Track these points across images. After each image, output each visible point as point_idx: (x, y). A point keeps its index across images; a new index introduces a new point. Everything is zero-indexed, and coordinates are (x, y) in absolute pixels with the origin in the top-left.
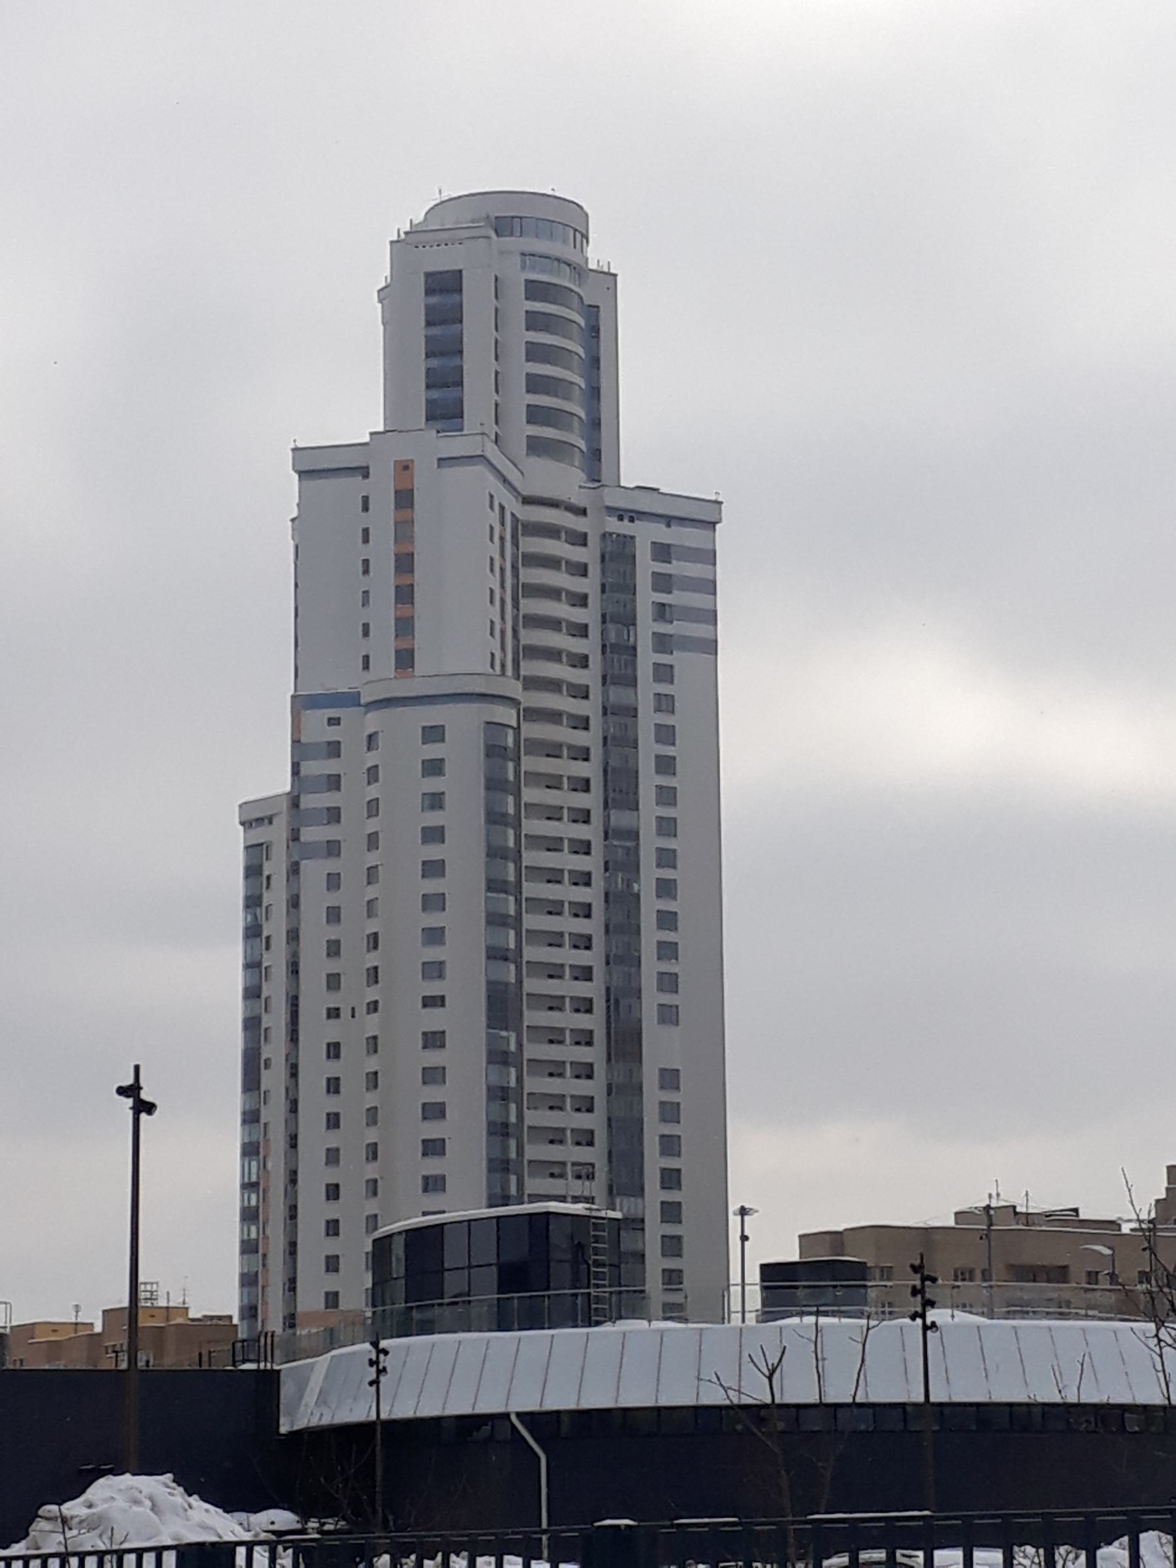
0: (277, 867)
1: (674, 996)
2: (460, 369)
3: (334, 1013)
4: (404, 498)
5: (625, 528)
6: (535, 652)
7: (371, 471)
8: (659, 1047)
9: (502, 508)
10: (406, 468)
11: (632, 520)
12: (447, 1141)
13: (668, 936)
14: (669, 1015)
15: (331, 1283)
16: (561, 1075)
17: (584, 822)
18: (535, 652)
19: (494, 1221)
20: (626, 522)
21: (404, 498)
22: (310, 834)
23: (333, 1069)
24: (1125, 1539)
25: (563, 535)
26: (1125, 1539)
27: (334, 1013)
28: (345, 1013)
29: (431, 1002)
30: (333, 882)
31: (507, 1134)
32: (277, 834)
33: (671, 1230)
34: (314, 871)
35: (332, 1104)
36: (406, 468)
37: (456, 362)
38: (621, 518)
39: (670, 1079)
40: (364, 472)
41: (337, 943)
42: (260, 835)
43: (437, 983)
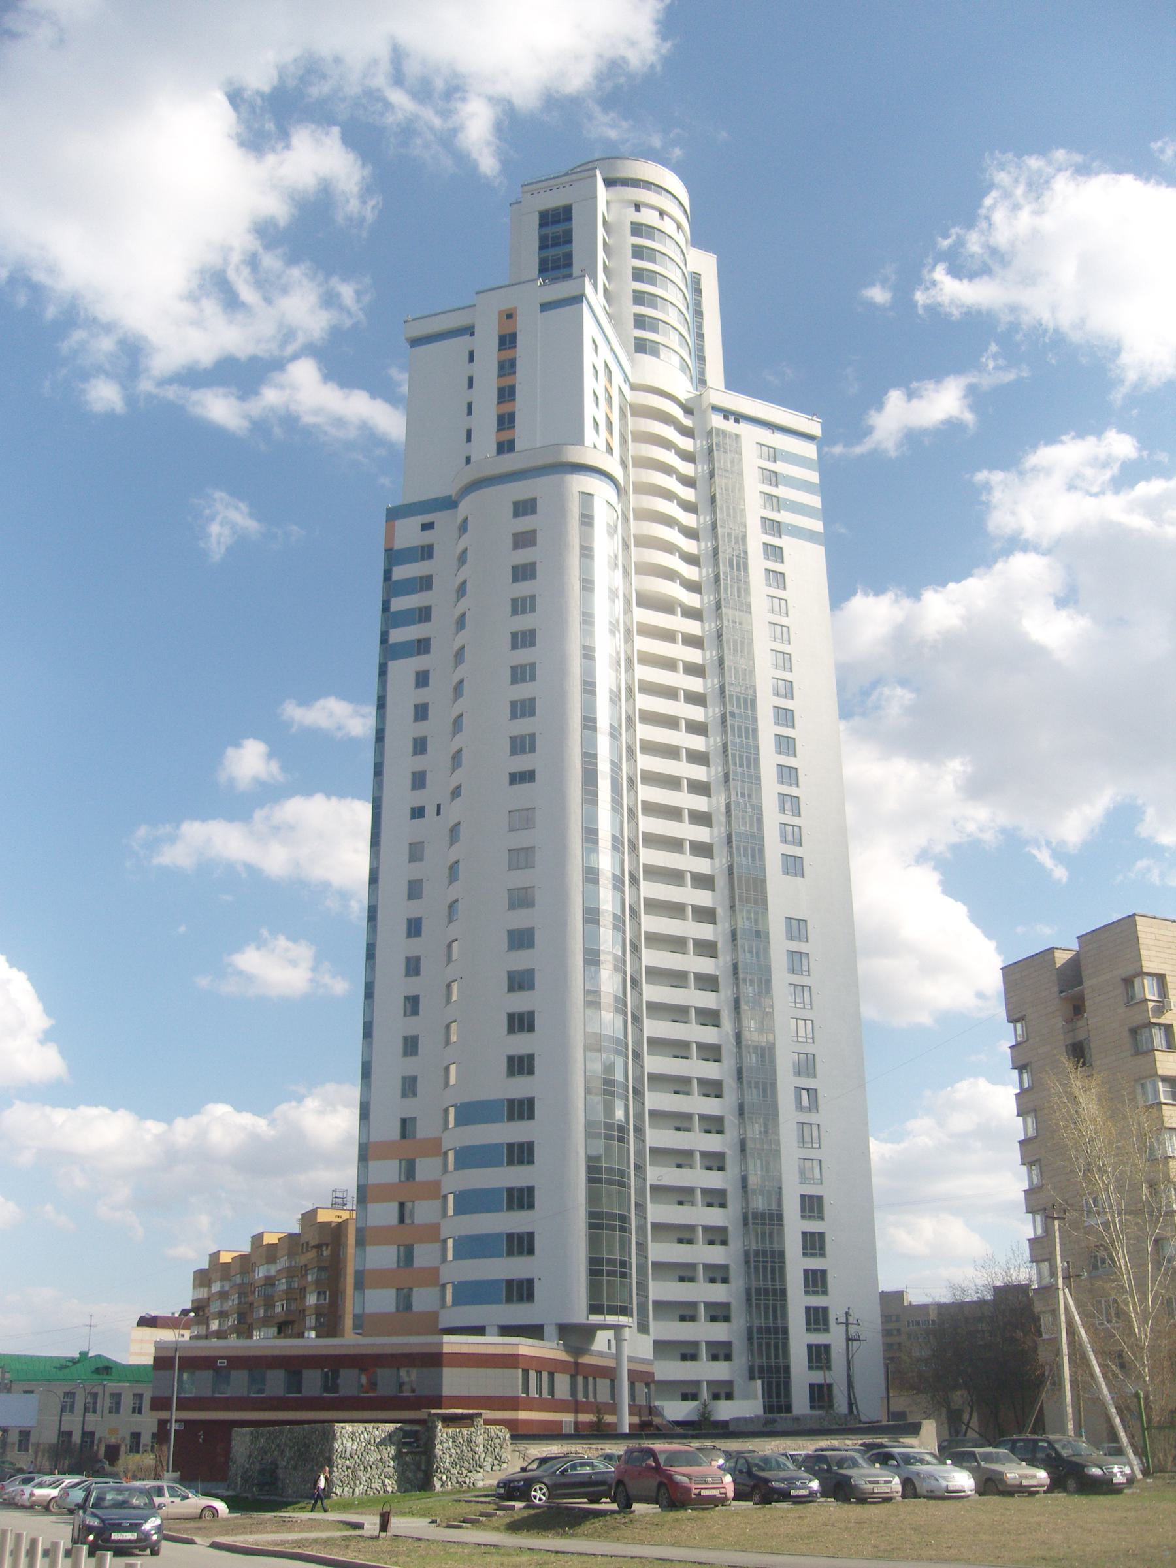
1: (823, 1298)
2: (571, 231)
4: (507, 341)
5: (730, 426)
6: (645, 542)
7: (476, 330)
8: (783, 897)
10: (510, 316)
11: (737, 421)
12: (536, 1281)
14: (794, 866)
16: (692, 1280)
17: (717, 1096)
18: (645, 542)
19: (588, 1054)
20: (732, 421)
21: (507, 341)
29: (517, 778)
30: (422, 679)
31: (612, 1094)
33: (814, 1264)
36: (510, 316)
37: (566, 248)
38: (726, 418)
39: (797, 928)
40: (470, 331)
43: (517, 697)
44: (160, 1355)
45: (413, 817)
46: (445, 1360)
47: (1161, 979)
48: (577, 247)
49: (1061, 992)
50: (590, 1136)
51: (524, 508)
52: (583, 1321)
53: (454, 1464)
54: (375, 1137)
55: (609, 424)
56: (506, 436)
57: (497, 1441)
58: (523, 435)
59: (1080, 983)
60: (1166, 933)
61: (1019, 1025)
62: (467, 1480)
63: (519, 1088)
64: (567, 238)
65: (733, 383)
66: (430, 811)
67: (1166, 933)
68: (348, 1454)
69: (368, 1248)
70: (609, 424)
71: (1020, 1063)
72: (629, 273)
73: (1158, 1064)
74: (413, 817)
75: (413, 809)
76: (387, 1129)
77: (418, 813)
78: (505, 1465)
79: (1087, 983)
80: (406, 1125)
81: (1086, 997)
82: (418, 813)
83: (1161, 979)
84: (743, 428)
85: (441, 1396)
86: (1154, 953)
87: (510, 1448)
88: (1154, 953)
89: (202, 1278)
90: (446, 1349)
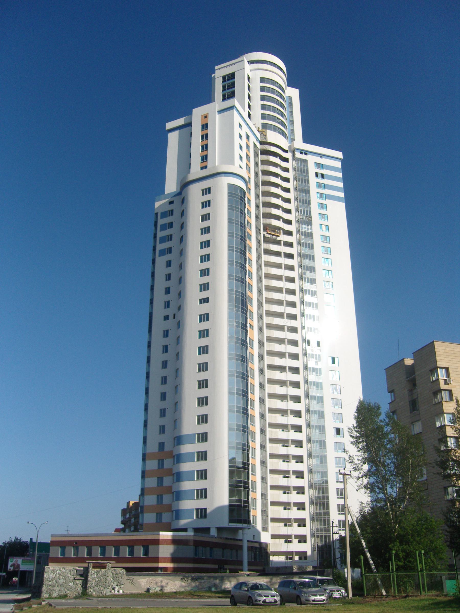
5: (303, 157)
10: (206, 117)
15: (162, 438)
21: (205, 126)
30: (169, 264)
44: (156, 546)
45: (165, 320)
46: (160, 543)
47: (447, 369)
48: (237, 89)
49: (407, 378)
50: (230, 448)
51: (207, 191)
52: (227, 526)
53: (97, 585)
54: (148, 451)
55: (248, 157)
56: (204, 164)
57: (120, 575)
58: (209, 163)
59: (414, 374)
60: (450, 349)
61: (392, 394)
62: (102, 592)
63: (202, 428)
64: (234, 85)
65: (306, 140)
66: (171, 317)
67: (450, 349)
68: (50, 580)
69: (145, 496)
70: (248, 157)
71: (393, 410)
72: (259, 98)
73: (444, 408)
74: (165, 320)
75: (165, 317)
76: (153, 447)
77: (166, 318)
78: (122, 586)
79: (417, 373)
80: (162, 445)
81: (416, 379)
82: (166, 318)
83: (447, 369)
84: (309, 158)
85: (158, 557)
86: (443, 358)
87: (126, 577)
88: (443, 358)
89: (124, 512)
90: (161, 538)
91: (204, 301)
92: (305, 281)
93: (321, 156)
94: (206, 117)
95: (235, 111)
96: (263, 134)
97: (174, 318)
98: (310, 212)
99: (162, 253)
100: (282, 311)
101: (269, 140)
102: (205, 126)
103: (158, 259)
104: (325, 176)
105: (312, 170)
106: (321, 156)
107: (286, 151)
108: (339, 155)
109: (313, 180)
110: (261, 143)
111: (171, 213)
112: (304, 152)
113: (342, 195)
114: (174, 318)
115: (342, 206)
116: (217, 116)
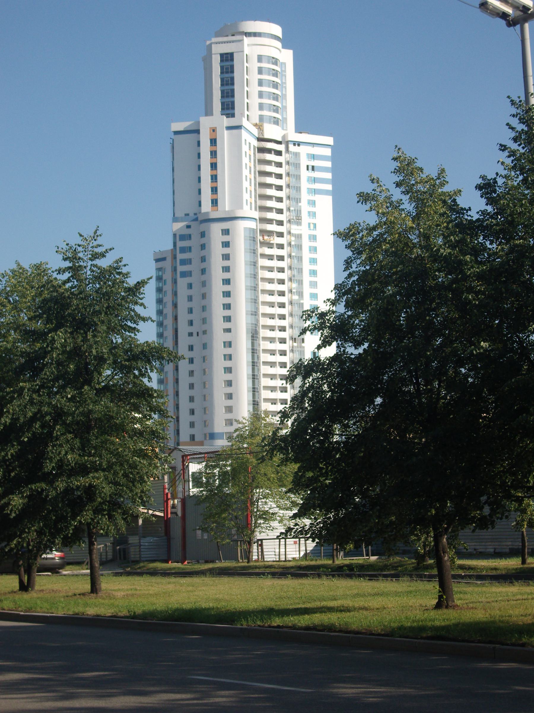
0: (168, 276)
3: (191, 334)
9: (250, 143)
10: (214, 131)
11: (299, 145)
13: (313, 244)
15: (192, 431)
22: (181, 268)
23: (191, 317)
24: (281, 37)
25: (273, 152)
26: (281, 37)
27: (191, 334)
28: (195, 334)
30: (190, 286)
32: (167, 264)
34: (182, 283)
35: (192, 418)
41: (192, 371)
42: (161, 264)
65: (299, 130)
75: (189, 333)
84: (303, 150)
91: (228, 330)
92: (294, 282)
93: (313, 144)
94: (214, 131)
95: (243, 131)
96: (259, 127)
97: (198, 335)
98: (300, 211)
99: (184, 274)
100: (274, 313)
101: (266, 136)
102: (213, 142)
103: (180, 280)
104: (315, 169)
105: (304, 162)
106: (313, 144)
107: (279, 143)
108: (330, 140)
109: (305, 174)
110: (260, 140)
111: (189, 237)
112: (297, 143)
113: (329, 187)
114: (198, 335)
115: (329, 199)
116: (226, 132)
